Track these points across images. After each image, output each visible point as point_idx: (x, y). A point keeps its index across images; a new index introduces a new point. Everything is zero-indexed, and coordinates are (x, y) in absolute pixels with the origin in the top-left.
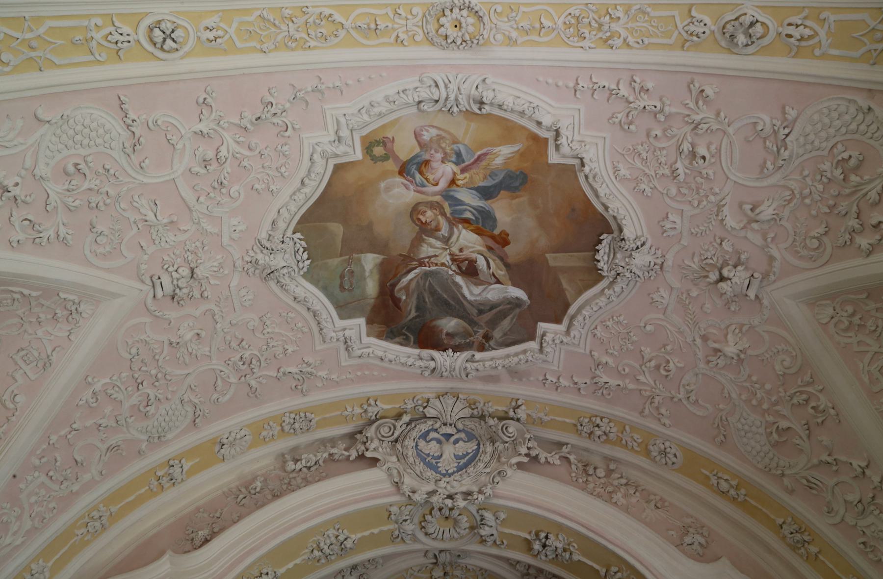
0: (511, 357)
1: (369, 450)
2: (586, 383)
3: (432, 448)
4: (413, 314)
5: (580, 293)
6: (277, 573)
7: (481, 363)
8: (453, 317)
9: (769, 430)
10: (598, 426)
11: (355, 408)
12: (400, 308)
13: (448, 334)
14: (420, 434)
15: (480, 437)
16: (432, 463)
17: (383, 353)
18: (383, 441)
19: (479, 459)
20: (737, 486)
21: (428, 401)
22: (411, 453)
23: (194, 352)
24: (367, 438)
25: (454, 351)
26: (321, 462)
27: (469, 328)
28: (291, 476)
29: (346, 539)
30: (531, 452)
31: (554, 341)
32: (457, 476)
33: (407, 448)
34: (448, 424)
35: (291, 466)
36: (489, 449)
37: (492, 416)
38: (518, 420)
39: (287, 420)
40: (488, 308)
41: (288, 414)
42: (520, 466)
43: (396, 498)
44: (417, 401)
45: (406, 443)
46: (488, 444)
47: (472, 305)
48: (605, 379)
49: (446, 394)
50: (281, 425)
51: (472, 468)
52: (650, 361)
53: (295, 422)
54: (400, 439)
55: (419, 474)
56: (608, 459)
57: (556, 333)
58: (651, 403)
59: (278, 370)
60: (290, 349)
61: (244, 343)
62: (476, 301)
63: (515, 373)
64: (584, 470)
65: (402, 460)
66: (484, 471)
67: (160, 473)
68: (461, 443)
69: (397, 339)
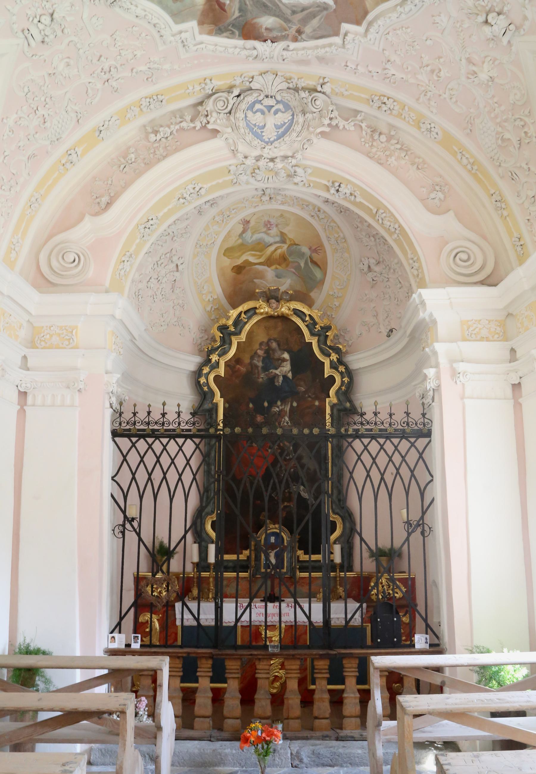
0: (319, 49)
1: (210, 123)
2: (378, 72)
3: (257, 119)
4: (237, 14)
5: (377, 4)
6: (158, 217)
7: (295, 52)
8: (271, 16)
9: (498, 136)
10: (385, 103)
11: (195, 86)
12: (224, 10)
13: (267, 29)
14: (248, 105)
15: (295, 108)
16: (258, 132)
17: (214, 47)
18: (220, 113)
19: (293, 129)
20: (473, 163)
21: (253, 78)
22: (242, 124)
23: (67, 75)
24: (207, 111)
25: (272, 42)
26: (174, 132)
27: (285, 25)
28: (155, 145)
29: (200, 189)
30: (332, 123)
31: (354, 40)
32: (276, 144)
33: (238, 120)
34: (269, 96)
35: (152, 137)
36: (301, 119)
37: (304, 89)
38: (324, 93)
39: (144, 104)
40: (300, 9)
41: (144, 99)
42: (323, 134)
43: (233, 161)
44: (244, 77)
45: (238, 115)
46: (300, 115)
47: (286, 6)
48: (393, 71)
49: (267, 72)
50: (140, 107)
51: (288, 137)
52: (427, 66)
53: (150, 104)
54: (233, 111)
55: (249, 142)
56: (392, 127)
57: (356, 34)
58: (425, 95)
59: (132, 70)
60: (139, 53)
61: (102, 59)
62: (289, 3)
63: (321, 59)
64: (372, 135)
65: (236, 131)
66: (296, 139)
67: (63, 161)
68: (280, 114)
69: (225, 34)
